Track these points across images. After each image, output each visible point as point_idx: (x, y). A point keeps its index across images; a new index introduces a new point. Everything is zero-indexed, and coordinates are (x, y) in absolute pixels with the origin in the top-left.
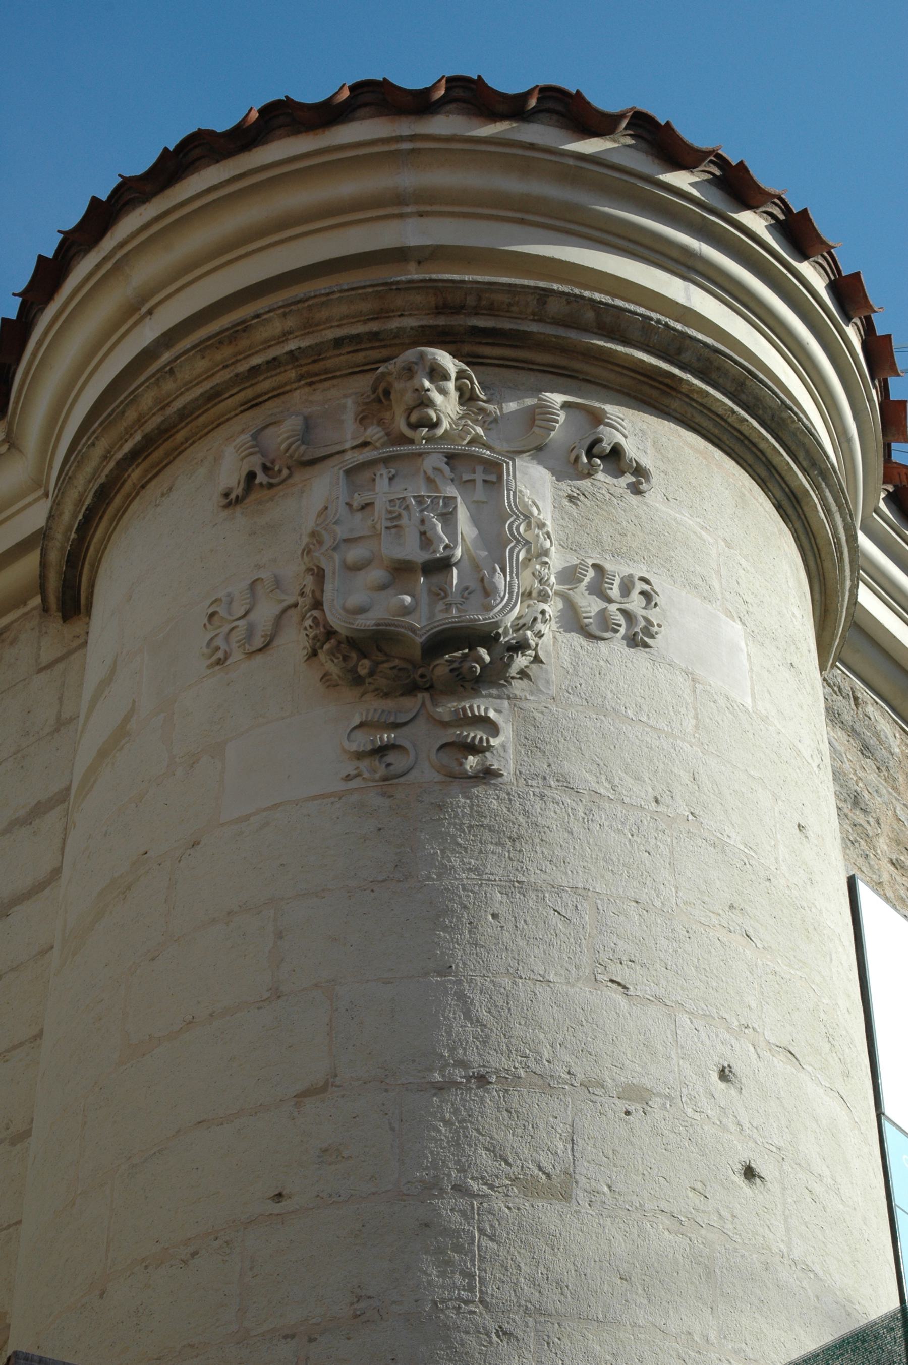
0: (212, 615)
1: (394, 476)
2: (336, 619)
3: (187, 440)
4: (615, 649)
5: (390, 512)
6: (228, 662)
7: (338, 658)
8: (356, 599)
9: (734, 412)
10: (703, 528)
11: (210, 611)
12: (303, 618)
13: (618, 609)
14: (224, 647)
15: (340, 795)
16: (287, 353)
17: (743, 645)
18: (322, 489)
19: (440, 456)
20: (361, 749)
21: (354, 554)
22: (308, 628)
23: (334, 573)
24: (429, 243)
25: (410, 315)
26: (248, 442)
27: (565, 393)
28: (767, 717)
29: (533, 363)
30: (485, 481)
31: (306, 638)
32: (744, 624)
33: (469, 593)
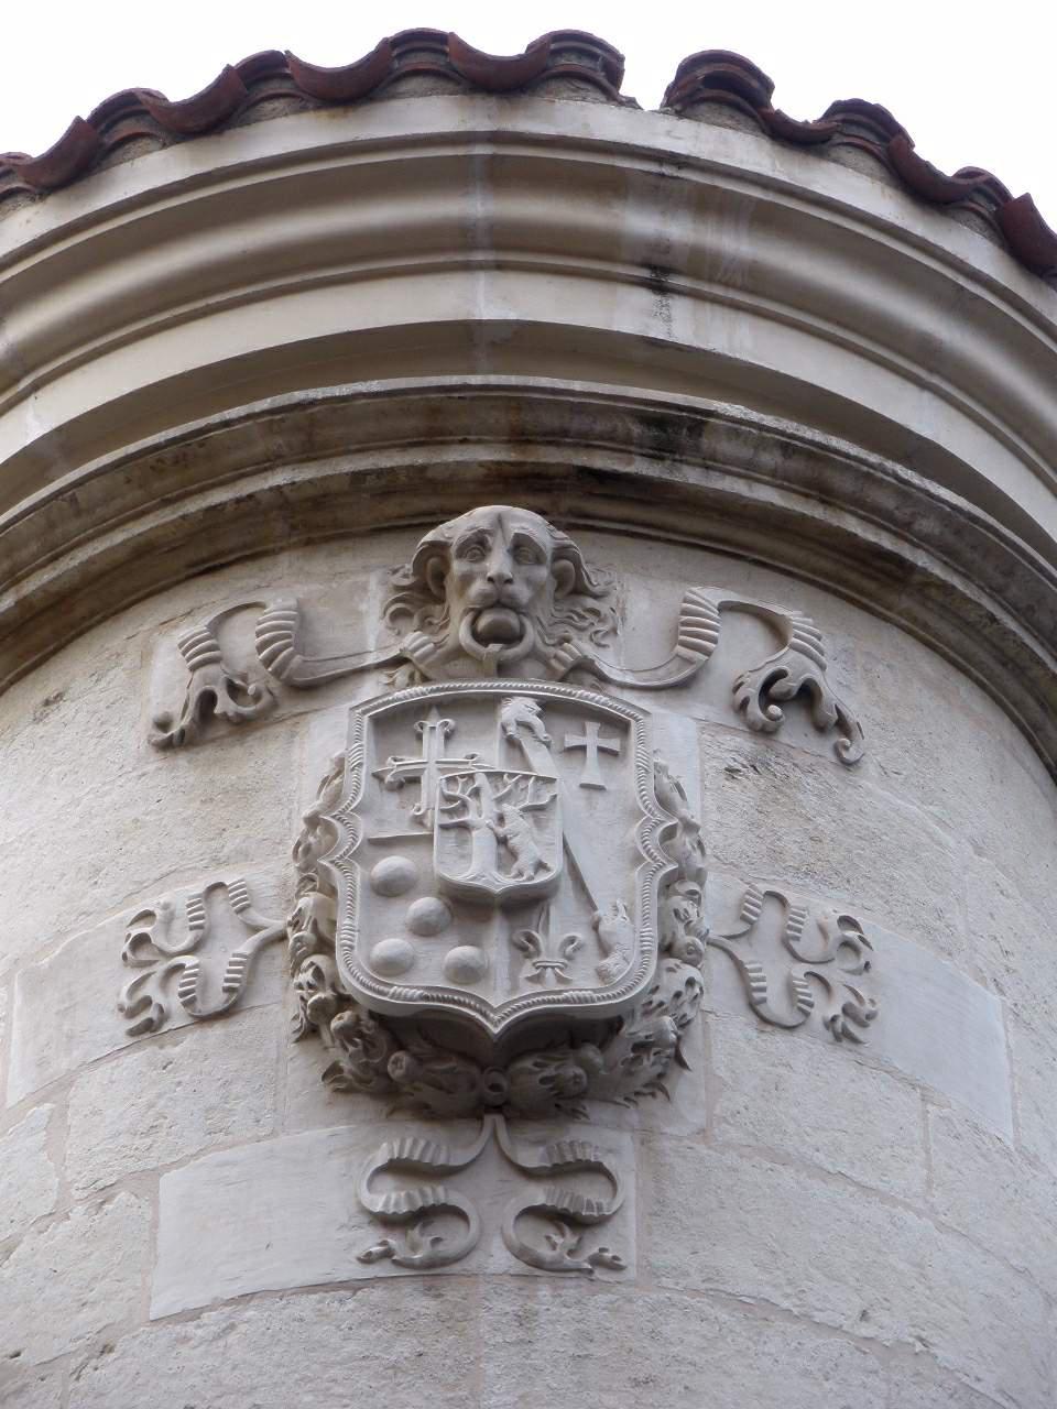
0: (141, 941)
1: (453, 731)
2: (353, 973)
3: (92, 614)
4: (807, 1053)
5: (449, 799)
6: (164, 1029)
7: (355, 1045)
8: (392, 944)
9: (993, 619)
10: (940, 822)
11: (136, 931)
12: (296, 968)
13: (807, 974)
14: (158, 998)
15: (353, 1286)
16: (271, 489)
17: (1001, 1031)
18: (329, 737)
19: (531, 702)
20: (391, 1210)
21: (390, 863)
22: (305, 986)
23: (353, 899)
24: (513, 316)
25: (479, 442)
26: (205, 631)
27: (723, 586)
28: (1036, 1157)
29: (675, 530)
30: (601, 750)
31: (301, 1004)
32: (1002, 992)
33: (575, 950)
